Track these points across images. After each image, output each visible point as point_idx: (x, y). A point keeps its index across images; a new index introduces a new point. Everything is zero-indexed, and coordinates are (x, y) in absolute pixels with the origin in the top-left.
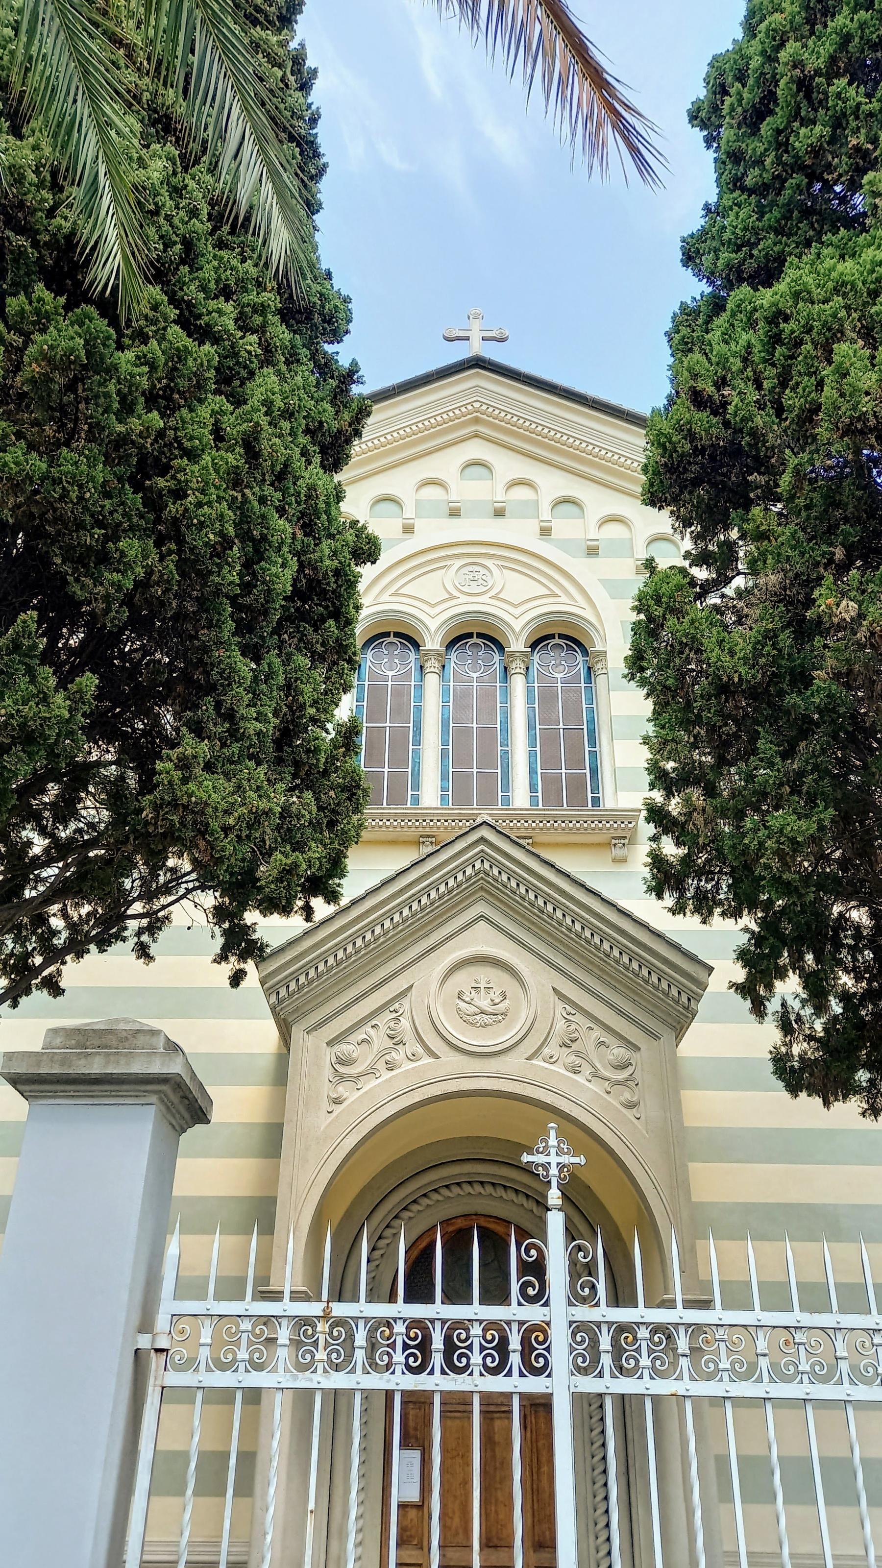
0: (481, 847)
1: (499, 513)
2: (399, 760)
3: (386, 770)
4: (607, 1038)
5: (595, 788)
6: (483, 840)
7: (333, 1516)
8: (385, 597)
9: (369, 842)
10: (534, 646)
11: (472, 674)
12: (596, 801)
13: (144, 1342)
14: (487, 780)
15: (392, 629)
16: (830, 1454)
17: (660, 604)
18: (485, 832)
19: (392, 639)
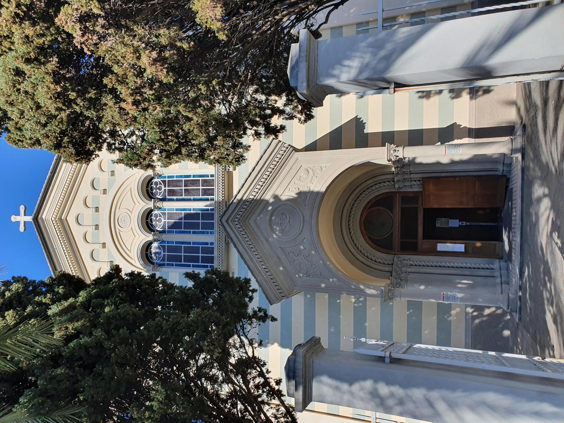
0: (229, 221)
1: (97, 209)
2: (196, 250)
3: (201, 188)
4: (292, 182)
5: (207, 176)
6: (227, 221)
7: (434, 272)
8: (132, 256)
9: (228, 266)
10: (153, 231)
11: (163, 222)
12: (212, 176)
13: (387, 360)
14: (205, 250)
15: (144, 252)
16: (407, 143)
17: (135, 158)
18: (224, 220)
19: (149, 220)
